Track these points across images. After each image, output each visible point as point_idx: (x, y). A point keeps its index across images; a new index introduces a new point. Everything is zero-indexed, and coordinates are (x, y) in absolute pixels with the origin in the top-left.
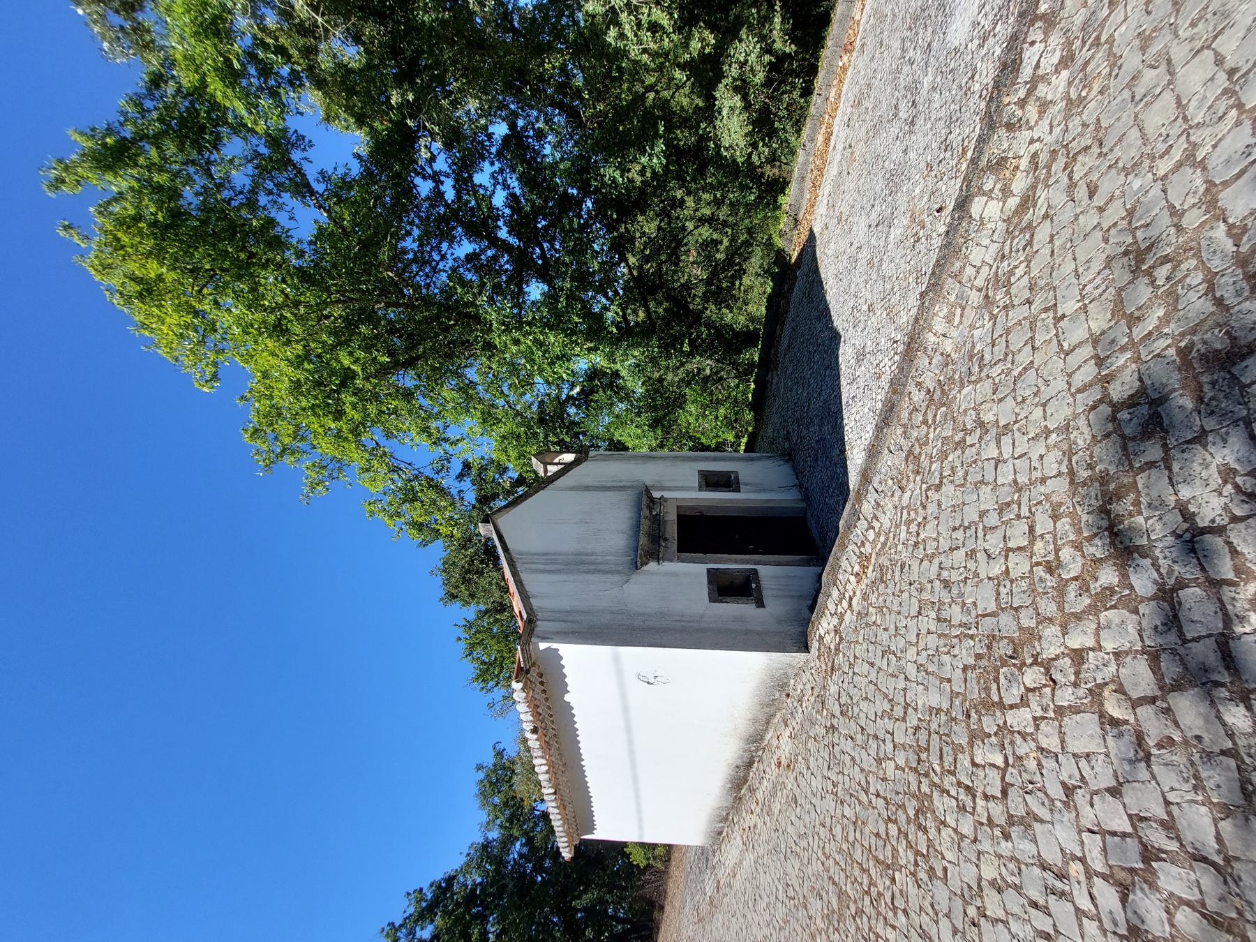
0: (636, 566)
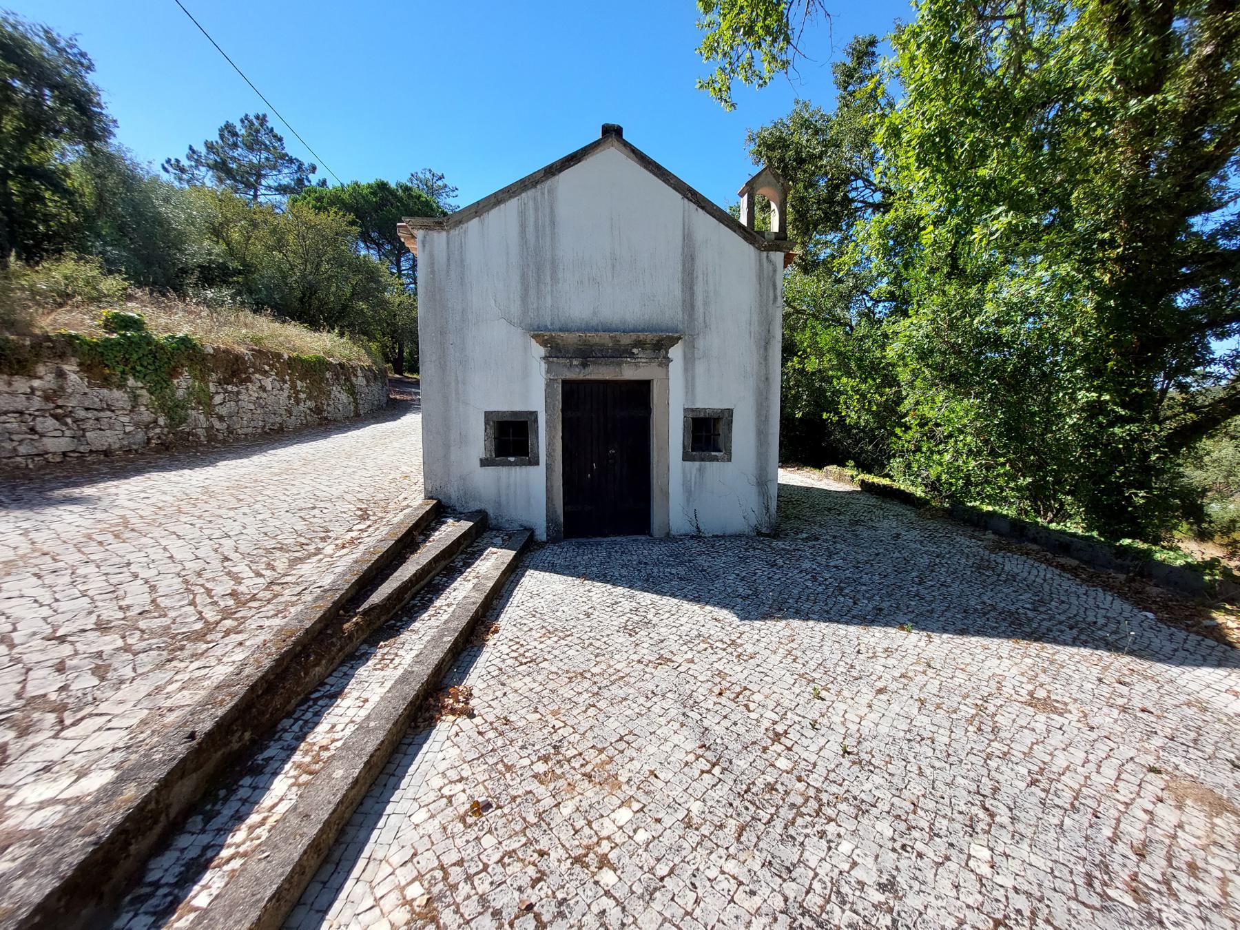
0: (542, 335)
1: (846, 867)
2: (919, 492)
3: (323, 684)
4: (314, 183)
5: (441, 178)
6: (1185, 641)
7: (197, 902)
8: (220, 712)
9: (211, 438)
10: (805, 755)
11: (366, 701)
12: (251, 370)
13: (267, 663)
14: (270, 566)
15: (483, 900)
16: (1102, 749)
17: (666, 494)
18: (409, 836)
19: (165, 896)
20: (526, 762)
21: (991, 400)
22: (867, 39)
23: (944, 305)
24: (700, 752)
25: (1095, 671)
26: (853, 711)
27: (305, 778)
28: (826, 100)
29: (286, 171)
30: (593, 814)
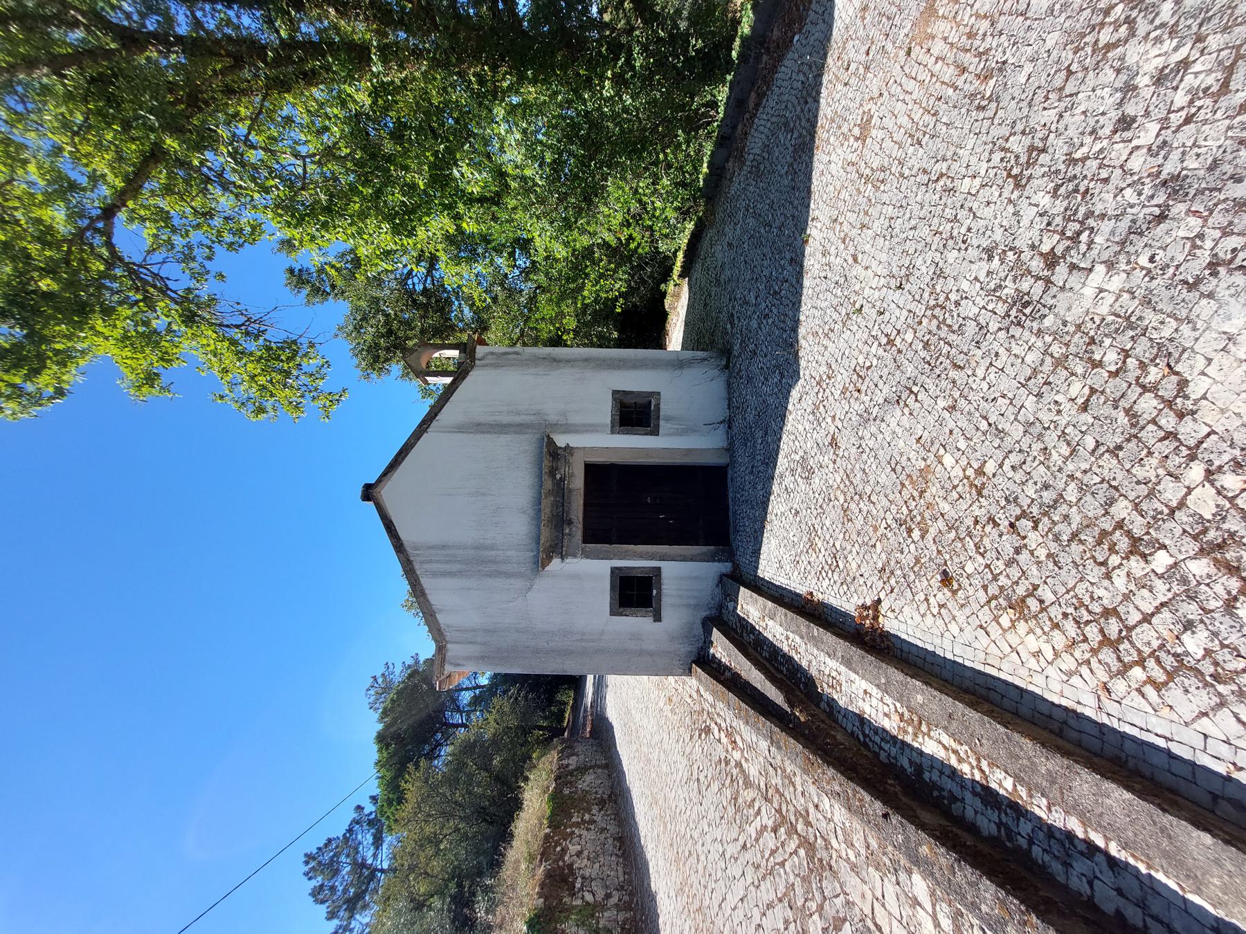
0: (541, 562)
1: (978, 285)
2: (690, 226)
3: (852, 733)
4: (373, 808)
5: (375, 678)
6: (817, 13)
7: (1010, 787)
8: (867, 798)
9: (627, 907)
10: (903, 319)
11: (865, 692)
12: (561, 863)
13: (831, 772)
14: (751, 805)
15: (1009, 564)
16: (895, 89)
17: (689, 451)
18: (968, 635)
19: (1006, 814)
20: (912, 547)
21: (609, 167)
22: (288, 275)
23: (525, 209)
24: (902, 404)
25: (839, 87)
26: (870, 282)
27: (924, 728)
28: (338, 311)
29: (360, 837)
30: (948, 486)
